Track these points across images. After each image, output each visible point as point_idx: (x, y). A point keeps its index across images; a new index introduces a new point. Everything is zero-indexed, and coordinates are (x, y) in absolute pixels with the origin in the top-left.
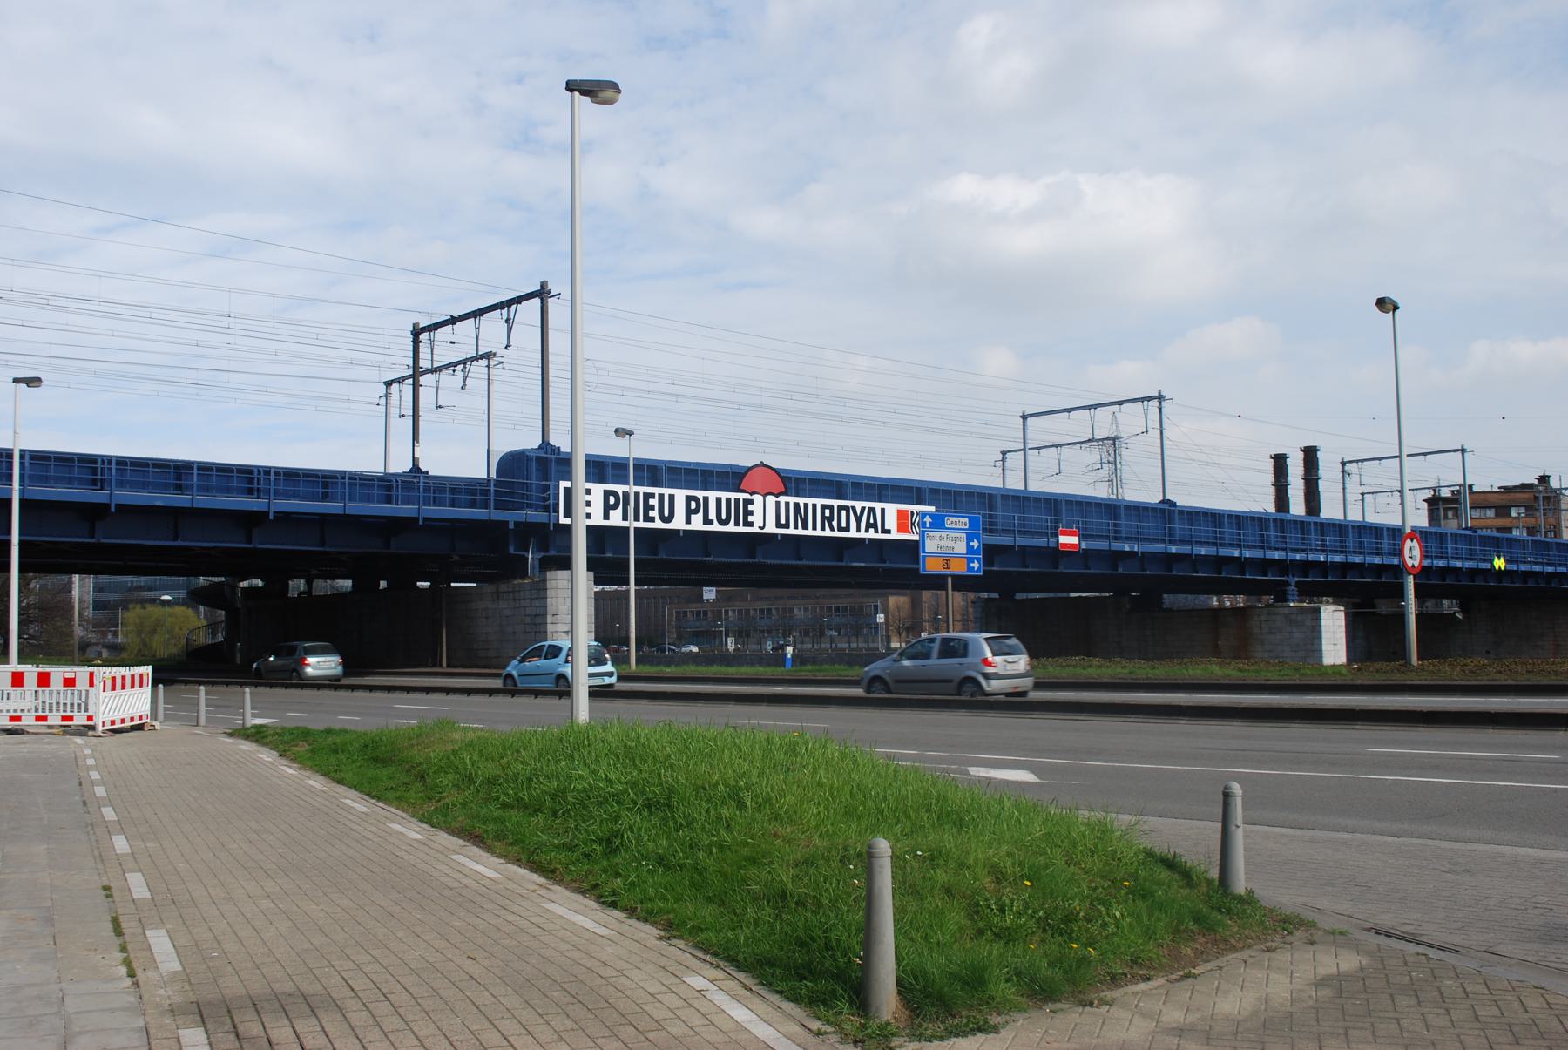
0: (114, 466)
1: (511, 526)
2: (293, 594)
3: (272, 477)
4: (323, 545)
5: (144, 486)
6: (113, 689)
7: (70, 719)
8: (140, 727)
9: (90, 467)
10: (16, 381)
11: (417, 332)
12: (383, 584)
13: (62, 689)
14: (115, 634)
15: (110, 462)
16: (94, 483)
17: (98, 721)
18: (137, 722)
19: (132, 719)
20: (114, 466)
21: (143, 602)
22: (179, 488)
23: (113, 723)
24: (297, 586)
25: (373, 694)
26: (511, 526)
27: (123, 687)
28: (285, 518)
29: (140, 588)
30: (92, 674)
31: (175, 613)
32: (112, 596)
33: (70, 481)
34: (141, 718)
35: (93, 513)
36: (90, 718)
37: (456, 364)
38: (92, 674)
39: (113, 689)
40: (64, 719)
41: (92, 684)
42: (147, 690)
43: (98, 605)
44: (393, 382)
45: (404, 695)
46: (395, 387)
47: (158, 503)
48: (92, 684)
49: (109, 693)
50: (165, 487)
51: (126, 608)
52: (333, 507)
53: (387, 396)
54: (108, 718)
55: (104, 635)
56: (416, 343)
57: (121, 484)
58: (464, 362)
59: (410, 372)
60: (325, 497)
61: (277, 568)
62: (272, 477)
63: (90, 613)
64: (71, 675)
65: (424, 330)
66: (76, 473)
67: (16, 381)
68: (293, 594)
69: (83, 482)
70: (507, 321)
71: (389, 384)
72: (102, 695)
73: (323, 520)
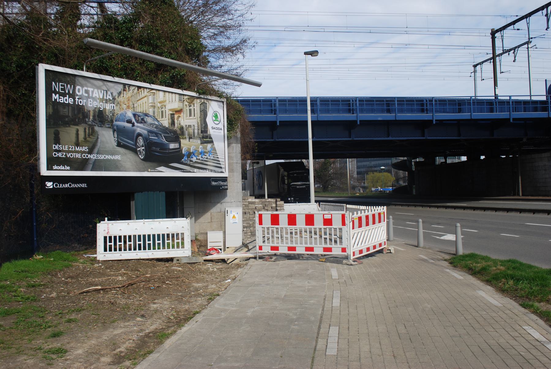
0: (358, 102)
1: (106, 219)
2: (437, 163)
3: (434, 102)
4: (460, 136)
5: (372, 111)
6: (360, 226)
7: (330, 250)
8: (381, 251)
9: (347, 104)
10: (306, 53)
11: (493, 33)
12: (482, 157)
13: (323, 227)
14: (364, 183)
15: (356, 101)
16: (349, 111)
17: (350, 252)
18: (378, 249)
19: (375, 247)
20: (358, 102)
21: (373, 171)
22: (389, 111)
23: (361, 252)
24: (439, 160)
25: (523, 215)
26: (106, 219)
27: (367, 224)
28: (441, 123)
29: (371, 167)
30: (343, 216)
31: (385, 176)
32: (362, 170)
33: (338, 111)
34: (380, 245)
35: (350, 125)
36: (344, 250)
37: (510, 50)
38: (343, 216)
39: (360, 226)
40: (326, 250)
41: (344, 224)
42: (384, 224)
43: (358, 173)
44: (477, 65)
45: (531, 215)
46: (478, 67)
47: (379, 119)
48: (344, 224)
49: (357, 230)
50: (382, 111)
51: (367, 174)
52: (465, 115)
53: (475, 72)
54: (356, 249)
55: (361, 183)
56: (493, 38)
57: (362, 111)
58: (514, 49)
59: (491, 56)
60: (460, 111)
61: (431, 149)
62: (434, 102)
63: (355, 175)
64: (329, 217)
65: (497, 31)
66: (341, 107)
67: (306, 53)
68: (437, 163)
69: (344, 111)
70: (547, 15)
71: (475, 66)
72: (352, 232)
73: (459, 123)
